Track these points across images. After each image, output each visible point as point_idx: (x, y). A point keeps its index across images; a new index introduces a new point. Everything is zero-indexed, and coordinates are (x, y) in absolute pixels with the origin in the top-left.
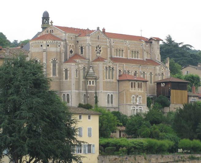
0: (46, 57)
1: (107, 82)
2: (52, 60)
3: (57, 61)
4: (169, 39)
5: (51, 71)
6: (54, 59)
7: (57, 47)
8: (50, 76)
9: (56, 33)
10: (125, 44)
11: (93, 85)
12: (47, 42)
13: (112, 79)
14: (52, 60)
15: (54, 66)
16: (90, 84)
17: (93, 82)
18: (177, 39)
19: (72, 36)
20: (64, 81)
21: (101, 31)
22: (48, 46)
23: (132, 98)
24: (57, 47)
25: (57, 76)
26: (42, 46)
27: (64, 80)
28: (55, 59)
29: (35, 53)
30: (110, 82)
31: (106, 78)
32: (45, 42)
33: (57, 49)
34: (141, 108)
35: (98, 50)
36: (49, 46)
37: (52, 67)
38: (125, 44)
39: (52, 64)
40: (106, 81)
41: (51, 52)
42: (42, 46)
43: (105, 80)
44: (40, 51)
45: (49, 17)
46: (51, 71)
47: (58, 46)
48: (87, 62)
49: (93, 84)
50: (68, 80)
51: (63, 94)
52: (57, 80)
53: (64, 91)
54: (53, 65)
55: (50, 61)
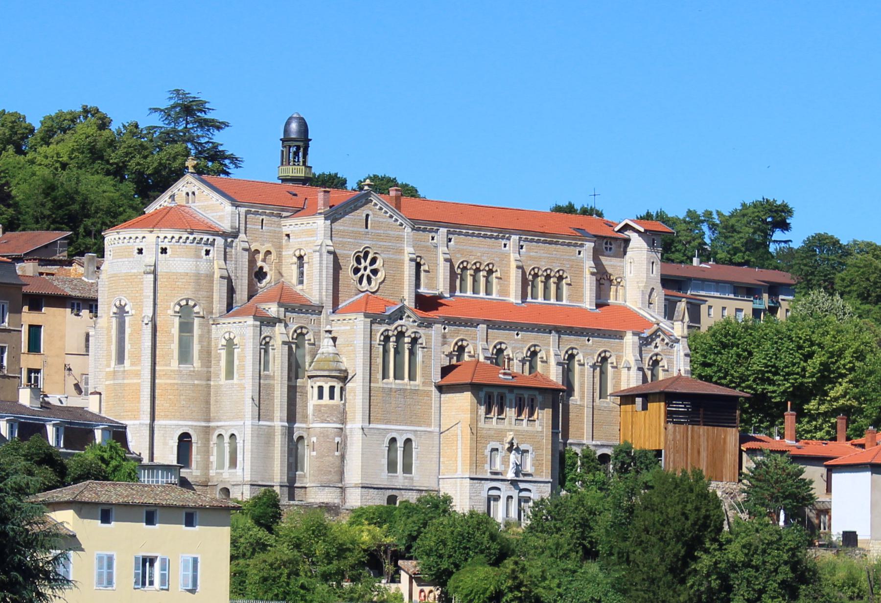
3: (196, 309)
7: (198, 257)
9: (206, 203)
11: (320, 402)
13: (412, 377)
14: (179, 304)
20: (222, 385)
22: (164, 251)
23: (487, 452)
26: (140, 251)
27: (223, 380)
30: (402, 391)
31: (385, 376)
32: (151, 238)
33: (197, 266)
34: (498, 489)
39: (177, 320)
42: (140, 251)
44: (135, 271)
45: (567, 204)
47: (204, 253)
50: (235, 381)
51: (217, 433)
52: (196, 382)
53: (219, 424)
55: (168, 308)
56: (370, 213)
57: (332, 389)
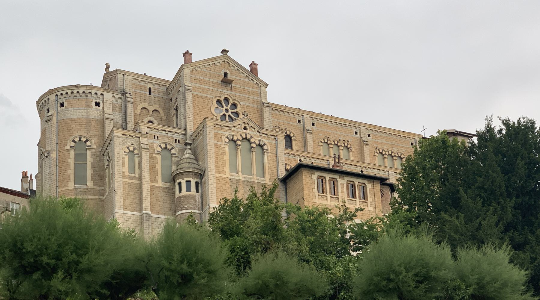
0: (58, 135)
1: (238, 181)
2: (74, 141)
3: (88, 143)
4: (506, 123)
5: (69, 161)
6: (77, 140)
8: (67, 186)
10: (356, 133)
11: (189, 193)
12: (57, 95)
14: (74, 141)
15: (80, 157)
16: (189, 189)
17: (188, 182)
18: (514, 120)
19: (150, 85)
21: (247, 70)
22: (62, 105)
24: (88, 106)
25: (90, 184)
28: (83, 139)
29: (50, 192)
35: (227, 110)
36: (65, 104)
37: (71, 161)
38: (356, 133)
39: (72, 153)
40: (231, 179)
41: (71, 119)
43: (228, 176)
46: (70, 172)
48: (177, 137)
49: (189, 189)
54: (76, 155)
56: (228, 72)
57: (188, 182)
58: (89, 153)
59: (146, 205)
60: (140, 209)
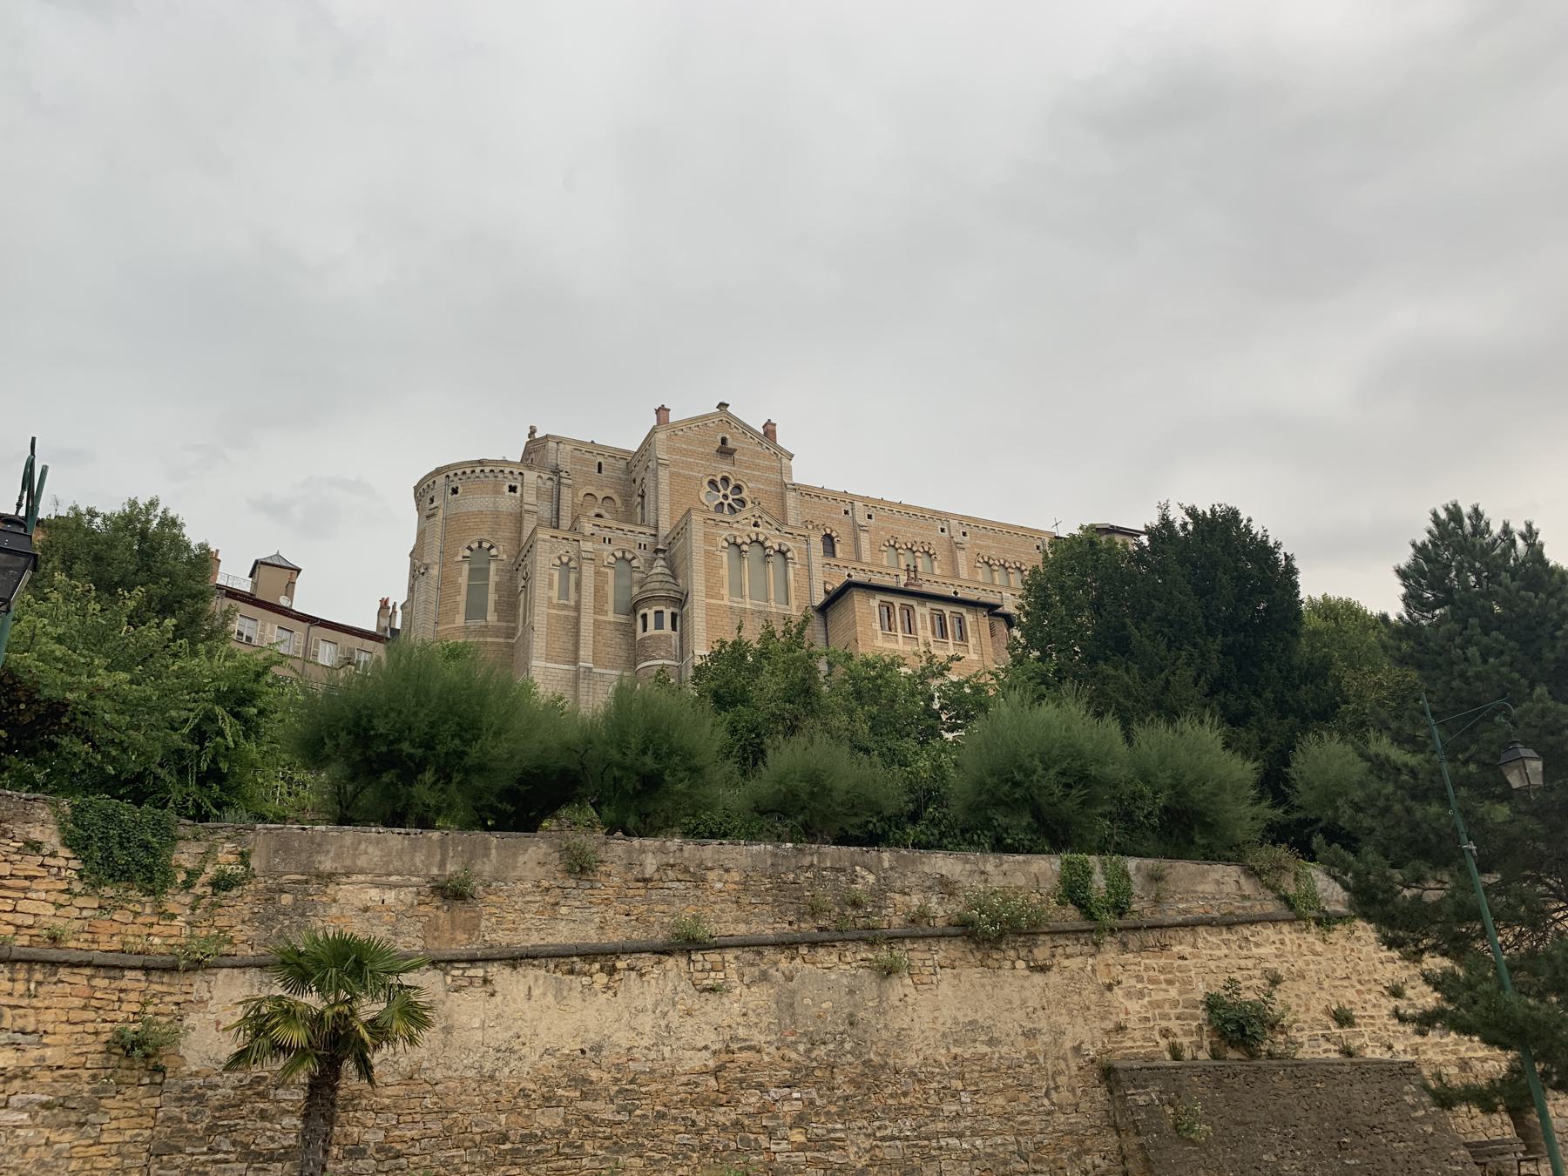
14: (469, 548)
22: (455, 491)
24: (497, 492)
39: (466, 567)
47: (506, 488)
49: (659, 625)
58: (493, 566)
59: (586, 652)
60: (575, 661)
